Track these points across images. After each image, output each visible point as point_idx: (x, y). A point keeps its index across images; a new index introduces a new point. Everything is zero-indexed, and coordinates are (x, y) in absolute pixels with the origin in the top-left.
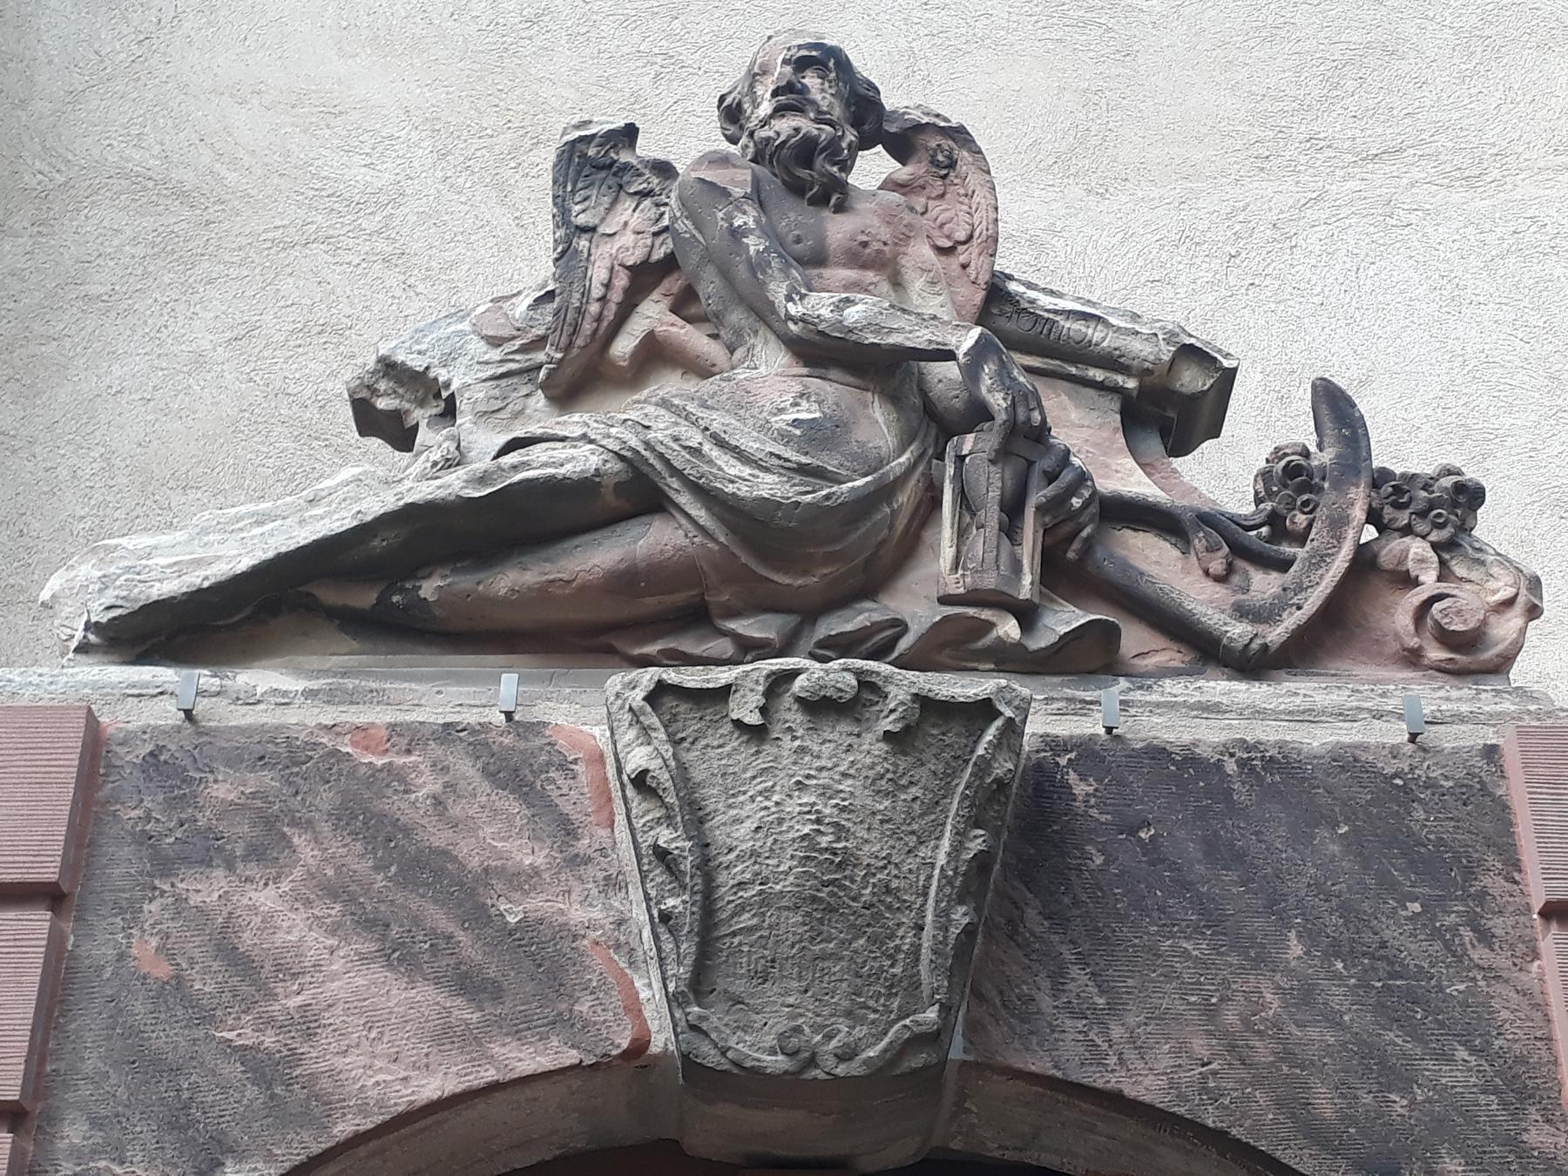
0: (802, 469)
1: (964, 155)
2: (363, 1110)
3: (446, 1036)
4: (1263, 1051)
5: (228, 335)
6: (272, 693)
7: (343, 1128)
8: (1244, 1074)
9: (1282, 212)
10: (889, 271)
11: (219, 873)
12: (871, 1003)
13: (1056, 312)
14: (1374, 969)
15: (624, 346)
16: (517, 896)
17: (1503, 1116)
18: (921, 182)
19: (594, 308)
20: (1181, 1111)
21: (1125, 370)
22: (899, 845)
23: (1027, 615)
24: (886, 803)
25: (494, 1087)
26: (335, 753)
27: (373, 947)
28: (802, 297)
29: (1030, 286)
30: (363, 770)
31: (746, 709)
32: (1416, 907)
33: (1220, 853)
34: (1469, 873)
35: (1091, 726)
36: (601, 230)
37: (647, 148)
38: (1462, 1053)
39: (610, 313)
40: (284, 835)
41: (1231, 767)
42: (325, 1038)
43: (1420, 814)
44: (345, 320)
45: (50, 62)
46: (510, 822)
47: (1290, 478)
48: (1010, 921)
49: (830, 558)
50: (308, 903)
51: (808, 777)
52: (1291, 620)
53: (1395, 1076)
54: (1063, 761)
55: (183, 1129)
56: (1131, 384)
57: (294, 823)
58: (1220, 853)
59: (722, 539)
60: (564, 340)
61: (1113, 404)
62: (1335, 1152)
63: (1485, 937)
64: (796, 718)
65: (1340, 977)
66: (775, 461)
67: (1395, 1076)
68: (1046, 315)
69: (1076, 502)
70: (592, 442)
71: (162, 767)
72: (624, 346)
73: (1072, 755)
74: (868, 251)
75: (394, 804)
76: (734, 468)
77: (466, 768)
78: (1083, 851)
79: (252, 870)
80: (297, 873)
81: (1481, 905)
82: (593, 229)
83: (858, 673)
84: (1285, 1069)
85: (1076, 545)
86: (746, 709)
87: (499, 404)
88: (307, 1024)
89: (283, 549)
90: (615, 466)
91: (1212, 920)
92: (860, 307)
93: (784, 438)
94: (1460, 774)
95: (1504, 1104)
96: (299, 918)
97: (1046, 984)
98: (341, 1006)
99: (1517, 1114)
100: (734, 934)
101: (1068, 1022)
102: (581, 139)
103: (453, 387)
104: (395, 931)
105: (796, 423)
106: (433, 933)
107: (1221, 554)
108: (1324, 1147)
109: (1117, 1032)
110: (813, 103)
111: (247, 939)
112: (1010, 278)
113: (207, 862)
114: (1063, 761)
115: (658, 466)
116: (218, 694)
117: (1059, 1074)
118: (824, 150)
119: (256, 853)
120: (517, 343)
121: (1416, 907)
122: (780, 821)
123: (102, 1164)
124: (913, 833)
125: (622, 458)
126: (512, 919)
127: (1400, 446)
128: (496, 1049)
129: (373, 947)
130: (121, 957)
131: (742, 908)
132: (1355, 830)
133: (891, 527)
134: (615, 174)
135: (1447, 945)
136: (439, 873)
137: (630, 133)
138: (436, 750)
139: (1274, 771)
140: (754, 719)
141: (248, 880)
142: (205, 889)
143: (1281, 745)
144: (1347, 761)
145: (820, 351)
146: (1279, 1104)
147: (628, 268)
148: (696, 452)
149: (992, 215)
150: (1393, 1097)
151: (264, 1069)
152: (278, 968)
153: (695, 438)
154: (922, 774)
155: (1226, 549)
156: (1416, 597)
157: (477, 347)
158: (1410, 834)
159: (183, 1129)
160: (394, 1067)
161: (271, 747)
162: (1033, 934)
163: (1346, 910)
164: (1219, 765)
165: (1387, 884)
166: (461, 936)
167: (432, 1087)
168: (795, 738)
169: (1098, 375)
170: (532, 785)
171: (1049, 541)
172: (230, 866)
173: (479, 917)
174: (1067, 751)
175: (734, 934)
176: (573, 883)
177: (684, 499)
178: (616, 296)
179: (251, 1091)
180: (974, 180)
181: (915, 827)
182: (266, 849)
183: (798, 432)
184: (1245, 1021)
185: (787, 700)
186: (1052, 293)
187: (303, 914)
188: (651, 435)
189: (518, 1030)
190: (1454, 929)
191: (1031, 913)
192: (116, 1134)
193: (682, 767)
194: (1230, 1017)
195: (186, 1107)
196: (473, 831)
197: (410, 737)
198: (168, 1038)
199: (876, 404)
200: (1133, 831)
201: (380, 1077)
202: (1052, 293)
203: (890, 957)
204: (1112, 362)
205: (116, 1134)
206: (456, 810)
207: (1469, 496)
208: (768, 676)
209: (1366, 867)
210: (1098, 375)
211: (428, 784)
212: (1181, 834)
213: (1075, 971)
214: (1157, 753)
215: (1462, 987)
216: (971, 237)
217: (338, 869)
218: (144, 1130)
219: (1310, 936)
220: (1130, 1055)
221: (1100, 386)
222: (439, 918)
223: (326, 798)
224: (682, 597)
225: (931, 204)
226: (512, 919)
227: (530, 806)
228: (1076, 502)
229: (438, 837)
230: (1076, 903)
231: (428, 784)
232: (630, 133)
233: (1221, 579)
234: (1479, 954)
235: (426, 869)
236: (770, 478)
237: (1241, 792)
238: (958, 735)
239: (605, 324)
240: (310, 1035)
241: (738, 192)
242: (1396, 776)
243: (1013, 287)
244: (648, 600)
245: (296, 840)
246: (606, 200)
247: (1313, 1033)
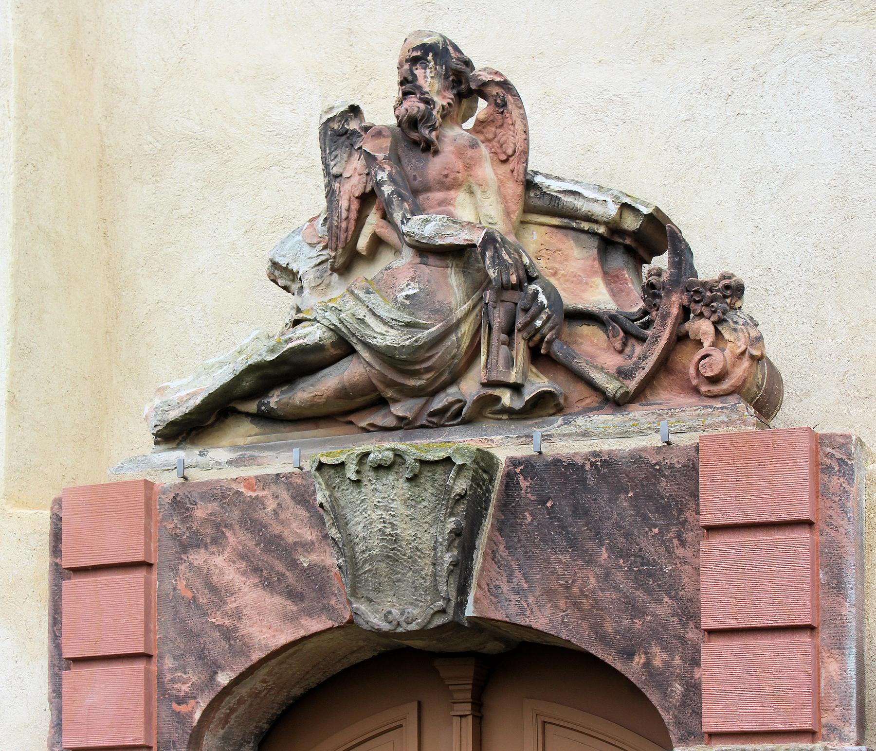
0: (408, 325)
1: (509, 98)
2: (260, 649)
3: (288, 618)
4: (586, 603)
5: (244, 230)
6: (216, 461)
7: (256, 657)
8: (578, 614)
9: (759, 58)
10: (465, 187)
11: (202, 550)
12: (419, 598)
13: (560, 192)
14: (635, 562)
15: (363, 243)
16: (306, 554)
17: (679, 626)
18: (492, 117)
19: (344, 225)
20: (553, 633)
21: (596, 222)
22: (420, 529)
23: (516, 388)
24: (412, 510)
25: (304, 639)
26: (237, 492)
27: (258, 580)
28: (408, 220)
29: (547, 176)
30: (248, 499)
31: (351, 473)
32: (656, 530)
33: (580, 511)
34: (681, 511)
35: (526, 451)
36: (345, 175)
38: (666, 599)
39: (352, 227)
40: (223, 532)
41: (588, 467)
42: (245, 620)
43: (664, 484)
44: (292, 213)
45: (144, 70)
46: (302, 521)
48: (493, 551)
49: (428, 370)
50: (234, 562)
51: (379, 502)
52: (640, 375)
53: (638, 612)
54: (518, 471)
55: (203, 659)
56: (601, 230)
57: (226, 526)
58: (580, 511)
59: (377, 368)
60: (334, 245)
61: (594, 243)
62: (611, 647)
63: (683, 543)
64: (372, 474)
65: (621, 567)
66: (394, 323)
67: (638, 612)
68: (555, 194)
69: (538, 323)
70: (318, 322)
71: (180, 505)
72: (363, 243)
73: (522, 467)
74: (449, 179)
75: (260, 515)
76: (380, 328)
77: (285, 496)
78: (523, 515)
79: (214, 549)
80: (229, 549)
81: (683, 527)
82: (341, 175)
83: (394, 450)
84: (595, 612)
85: (544, 346)
86: (351, 473)
87: (319, 281)
88: (238, 614)
89: (211, 392)
90: (328, 334)
91: (573, 544)
92: (434, 223)
93: (402, 307)
94: (684, 460)
95: (680, 621)
96: (231, 569)
97: (505, 580)
98: (249, 606)
99: (684, 626)
100: (365, 573)
101: (513, 597)
102: (329, 120)
103: (300, 274)
104: (265, 573)
105: (407, 297)
106: (277, 573)
107: (619, 338)
108: (606, 645)
109: (531, 600)
110: (420, 88)
111: (215, 579)
112: (536, 173)
113: (198, 546)
114: (518, 471)
115: (346, 331)
116: (196, 466)
117: (508, 620)
118: (421, 120)
119: (215, 541)
120: (322, 245)
121: (656, 530)
122: (371, 523)
123: (179, 674)
124: (427, 522)
125: (331, 330)
126: (305, 565)
128: (303, 622)
129: (258, 580)
130: (175, 589)
131: (365, 561)
132: (636, 494)
133: (458, 347)
134: (348, 138)
135: (667, 548)
136: (278, 545)
137: (354, 111)
138: (274, 488)
139: (605, 467)
140: (354, 477)
141: (213, 553)
142: (198, 557)
143: (610, 452)
144: (637, 459)
145: (426, 251)
146: (591, 627)
147: (357, 198)
148: (362, 321)
149: (524, 136)
150: (636, 621)
151: (228, 634)
152: (227, 591)
153: (361, 312)
154: (426, 495)
155: (622, 334)
156: (702, 352)
157: (306, 249)
158: (659, 493)
159: (203, 659)
160: (270, 631)
161: (215, 491)
162: (501, 557)
163: (628, 535)
164: (583, 467)
165: (645, 519)
166: (288, 574)
167: (283, 639)
168: (372, 484)
169: (585, 226)
170: (309, 502)
171: (531, 344)
172: (206, 548)
173: (294, 564)
174: (520, 465)
175: (365, 573)
176: (326, 547)
177: (359, 348)
178: (353, 215)
179: (223, 643)
180: (515, 113)
181: (427, 520)
182: (218, 540)
183: (408, 302)
184: (581, 591)
185: (367, 467)
186: (558, 178)
187: (233, 567)
188: (343, 315)
189: (310, 613)
190: (670, 540)
191: (501, 547)
192: (182, 662)
193: (336, 500)
194: (575, 590)
195: (203, 650)
196: (289, 525)
197: (263, 481)
198: (194, 623)
199: (453, 275)
200: (544, 503)
201: (266, 635)
202: (558, 178)
203: (424, 578)
204: (588, 218)
205: (182, 662)
206: (282, 516)
207: (737, 290)
208: (357, 456)
209: (638, 513)
210: (585, 226)
211: (271, 505)
212: (563, 503)
213: (517, 573)
214: (557, 462)
215: (670, 568)
216: (515, 151)
217: (243, 546)
218: (191, 660)
219: (611, 548)
220: (535, 609)
221: (587, 232)
222: (280, 566)
223: (236, 514)
224: (373, 396)
225: (498, 131)
226: (305, 565)
227: (309, 512)
228: (538, 323)
229: (276, 529)
230: (519, 541)
231: (271, 505)
233: (621, 352)
234: (680, 552)
235: (274, 544)
236: (393, 332)
237: (591, 480)
238: (440, 474)
239: (350, 233)
240: (240, 619)
241: (380, 156)
242: (656, 464)
243: (538, 179)
244: (359, 400)
245: (227, 534)
246: (345, 155)
247: (607, 594)
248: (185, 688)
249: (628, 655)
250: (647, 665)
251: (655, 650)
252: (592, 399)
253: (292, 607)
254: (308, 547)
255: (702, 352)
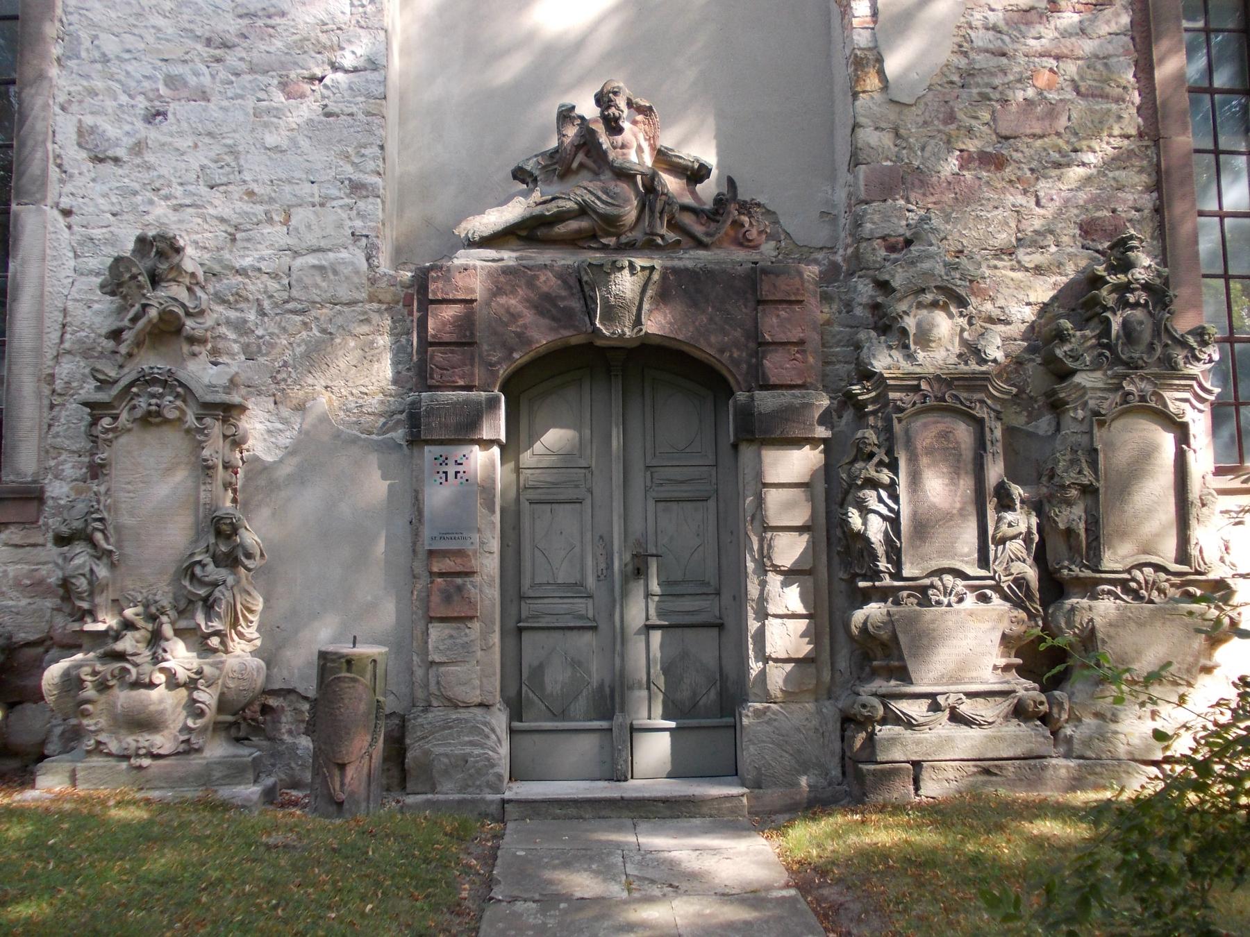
3: (551, 329)
15: (575, 165)
37: (578, 111)
47: (720, 201)
72: (575, 165)
88: (525, 326)
90: (576, 206)
119: (512, 292)
127: (743, 195)
139: (438, 801)
173: (556, 306)
189: (565, 328)
219: (713, 307)
222: (548, 306)
232: (573, 107)
248: (494, 359)
249: (722, 351)
250: (731, 356)
251: (734, 350)
252: (691, 243)
253: (554, 324)
254: (563, 298)
255: (744, 230)
